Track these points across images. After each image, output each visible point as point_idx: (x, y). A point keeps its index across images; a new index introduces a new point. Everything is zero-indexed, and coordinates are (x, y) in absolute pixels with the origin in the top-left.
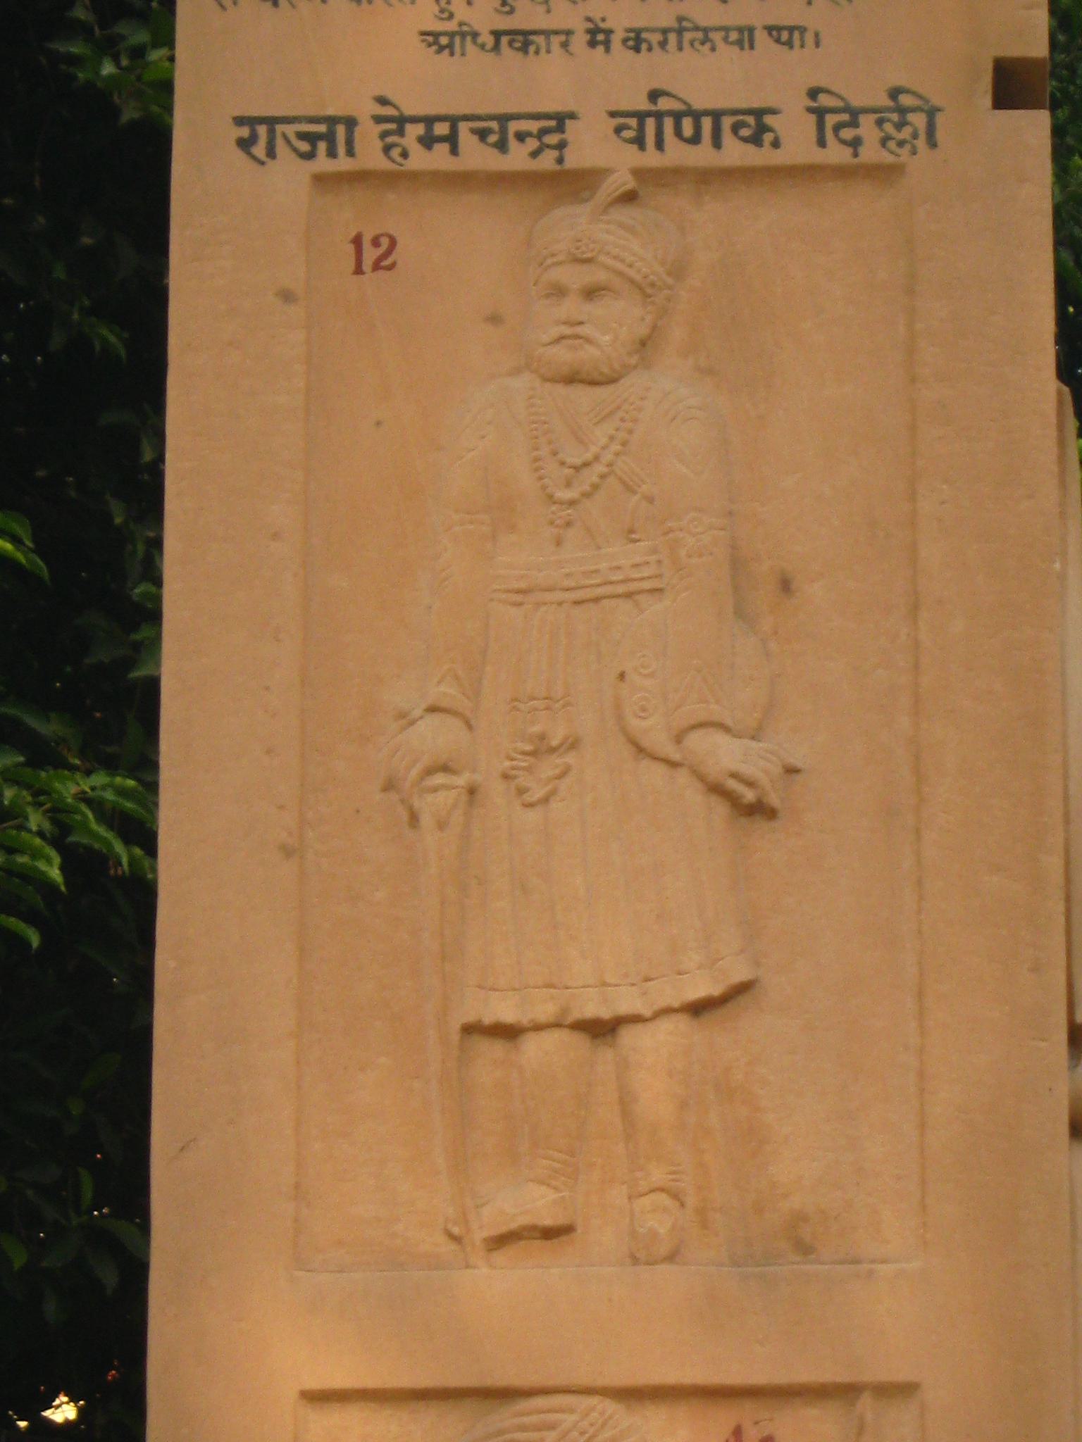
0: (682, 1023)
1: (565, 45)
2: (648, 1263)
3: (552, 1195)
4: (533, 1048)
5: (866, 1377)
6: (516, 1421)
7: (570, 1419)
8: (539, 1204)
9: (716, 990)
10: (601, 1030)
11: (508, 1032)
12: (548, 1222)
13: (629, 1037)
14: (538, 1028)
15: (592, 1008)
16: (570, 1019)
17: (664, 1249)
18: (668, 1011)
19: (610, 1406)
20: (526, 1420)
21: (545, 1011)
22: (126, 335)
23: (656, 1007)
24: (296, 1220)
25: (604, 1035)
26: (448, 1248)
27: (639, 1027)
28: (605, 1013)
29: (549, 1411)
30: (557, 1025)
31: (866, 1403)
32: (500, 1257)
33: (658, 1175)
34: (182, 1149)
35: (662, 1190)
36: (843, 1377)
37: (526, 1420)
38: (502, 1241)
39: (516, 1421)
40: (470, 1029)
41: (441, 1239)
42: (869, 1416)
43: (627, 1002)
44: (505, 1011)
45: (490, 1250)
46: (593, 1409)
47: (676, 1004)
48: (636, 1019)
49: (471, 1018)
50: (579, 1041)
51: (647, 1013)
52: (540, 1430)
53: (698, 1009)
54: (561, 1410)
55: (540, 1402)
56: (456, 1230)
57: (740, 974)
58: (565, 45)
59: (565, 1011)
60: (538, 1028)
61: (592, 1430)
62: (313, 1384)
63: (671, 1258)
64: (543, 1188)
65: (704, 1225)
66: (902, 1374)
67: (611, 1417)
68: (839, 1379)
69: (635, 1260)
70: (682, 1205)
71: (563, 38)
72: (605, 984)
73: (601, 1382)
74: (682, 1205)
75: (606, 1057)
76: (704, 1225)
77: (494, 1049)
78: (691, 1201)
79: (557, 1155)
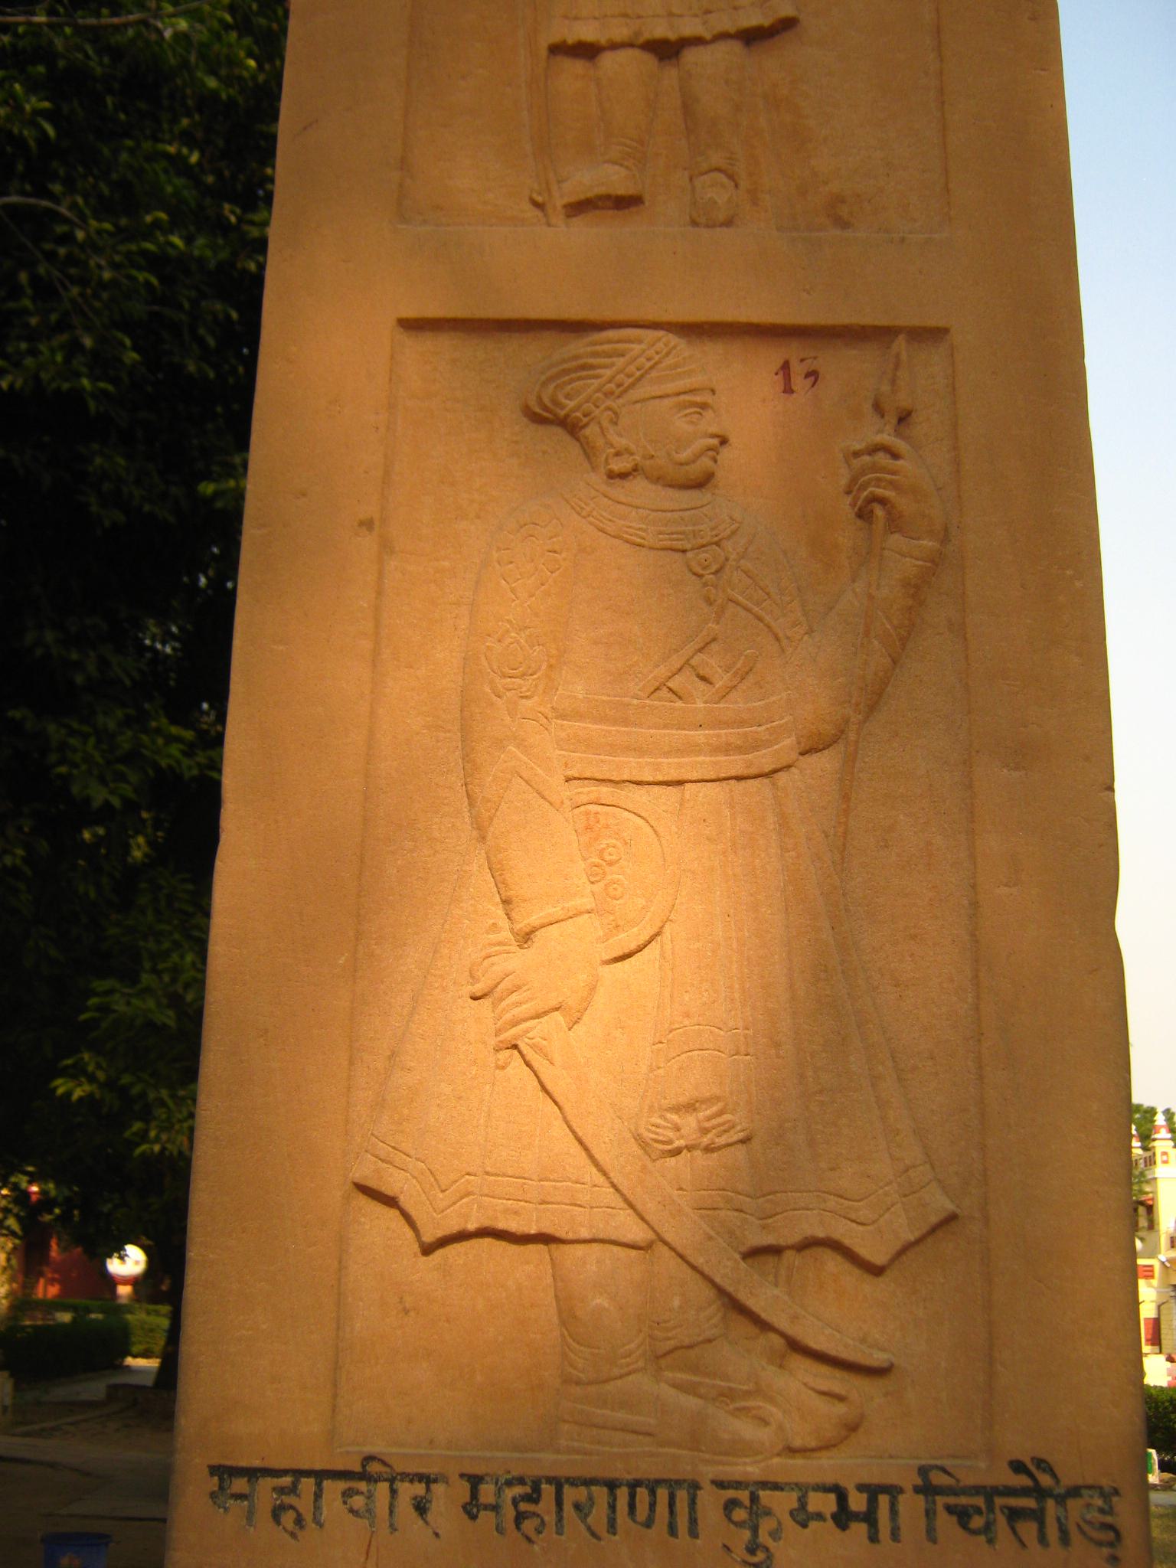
0: (737, 46)
1: (421, 1507)
2: (707, 226)
3: (623, 172)
4: (608, 61)
5: (900, 322)
6: (589, 349)
7: (637, 348)
8: (615, 179)
9: (766, 22)
10: (666, 50)
11: (587, 51)
12: (621, 192)
13: (690, 56)
14: (614, 46)
15: (660, 30)
16: (641, 40)
17: (721, 217)
18: (724, 36)
19: (673, 339)
20: (599, 348)
21: (620, 31)
22: (269, 171)
23: (715, 32)
24: (401, 185)
25: (669, 58)
26: (532, 213)
27: (701, 49)
28: (672, 36)
29: (618, 342)
30: (630, 45)
31: (900, 343)
32: (576, 221)
33: (716, 158)
34: (305, 128)
35: (719, 170)
36: (882, 321)
37: (599, 348)
38: (579, 208)
39: (589, 349)
40: (556, 49)
41: (527, 206)
42: (904, 356)
43: (690, 27)
44: (587, 32)
45: (568, 216)
46: (659, 339)
47: (732, 30)
48: (698, 41)
49: (556, 38)
50: (649, 60)
51: (708, 36)
52: (610, 357)
53: (751, 37)
54: (630, 341)
55: (611, 334)
56: (539, 199)
57: (787, 11)
58: (421, 1507)
59: (638, 34)
60: (614, 46)
61: (657, 358)
62: (410, 313)
63: (728, 223)
64: (617, 167)
65: (755, 202)
66: (933, 319)
67: (675, 347)
68: (877, 323)
69: (694, 223)
70: (736, 186)
71: (419, 1489)
72: (671, 14)
73: (665, 317)
74: (736, 186)
75: (670, 75)
76: (755, 202)
77: (576, 67)
78: (744, 184)
79: (628, 142)
